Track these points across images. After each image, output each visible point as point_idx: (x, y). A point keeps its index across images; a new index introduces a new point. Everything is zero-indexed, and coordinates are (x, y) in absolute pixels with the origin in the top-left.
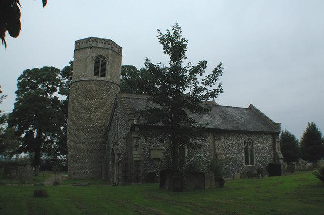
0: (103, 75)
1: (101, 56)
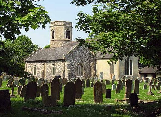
0: (54, 38)
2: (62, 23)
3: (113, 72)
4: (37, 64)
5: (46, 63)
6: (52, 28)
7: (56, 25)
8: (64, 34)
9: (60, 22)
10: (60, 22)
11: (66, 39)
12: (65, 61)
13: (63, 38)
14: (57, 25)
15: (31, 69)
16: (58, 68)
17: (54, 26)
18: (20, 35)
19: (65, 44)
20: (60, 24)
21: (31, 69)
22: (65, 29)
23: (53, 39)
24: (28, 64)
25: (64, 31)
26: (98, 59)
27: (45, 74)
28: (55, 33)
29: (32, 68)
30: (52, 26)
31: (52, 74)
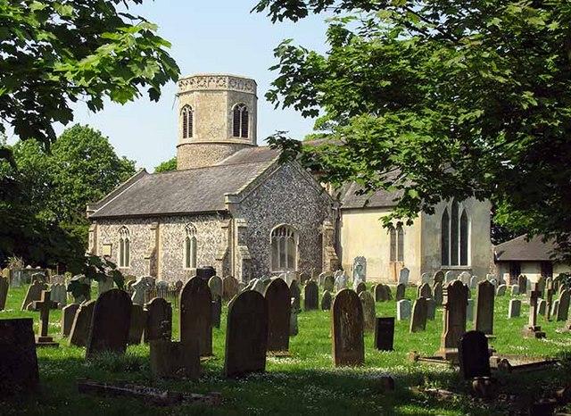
0: (191, 135)
1: (188, 106)
2: (221, 82)
3: (401, 257)
4: (131, 227)
5: (161, 225)
6: (186, 100)
7: (200, 88)
8: (226, 120)
9: (211, 77)
10: (212, 77)
11: (235, 140)
12: (232, 217)
13: (224, 136)
14: (203, 88)
15: (111, 245)
16: (205, 240)
17: (192, 92)
18: (71, 124)
19: (230, 157)
20: (213, 85)
21: (111, 245)
22: (231, 105)
23: (188, 140)
24: (99, 226)
25: (225, 110)
26: (348, 210)
27: (160, 262)
28: (194, 118)
29: (112, 242)
30: (185, 93)
31: (184, 262)
